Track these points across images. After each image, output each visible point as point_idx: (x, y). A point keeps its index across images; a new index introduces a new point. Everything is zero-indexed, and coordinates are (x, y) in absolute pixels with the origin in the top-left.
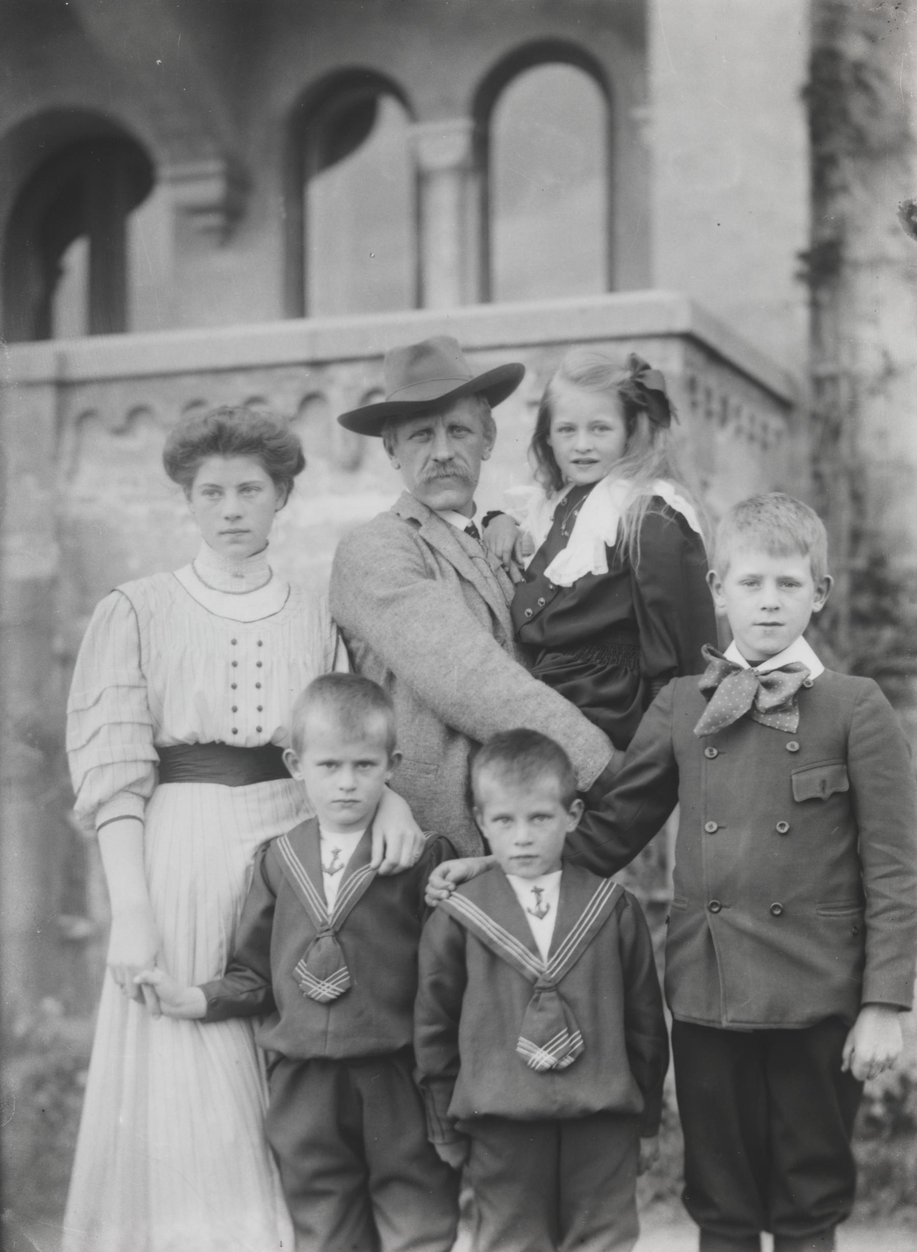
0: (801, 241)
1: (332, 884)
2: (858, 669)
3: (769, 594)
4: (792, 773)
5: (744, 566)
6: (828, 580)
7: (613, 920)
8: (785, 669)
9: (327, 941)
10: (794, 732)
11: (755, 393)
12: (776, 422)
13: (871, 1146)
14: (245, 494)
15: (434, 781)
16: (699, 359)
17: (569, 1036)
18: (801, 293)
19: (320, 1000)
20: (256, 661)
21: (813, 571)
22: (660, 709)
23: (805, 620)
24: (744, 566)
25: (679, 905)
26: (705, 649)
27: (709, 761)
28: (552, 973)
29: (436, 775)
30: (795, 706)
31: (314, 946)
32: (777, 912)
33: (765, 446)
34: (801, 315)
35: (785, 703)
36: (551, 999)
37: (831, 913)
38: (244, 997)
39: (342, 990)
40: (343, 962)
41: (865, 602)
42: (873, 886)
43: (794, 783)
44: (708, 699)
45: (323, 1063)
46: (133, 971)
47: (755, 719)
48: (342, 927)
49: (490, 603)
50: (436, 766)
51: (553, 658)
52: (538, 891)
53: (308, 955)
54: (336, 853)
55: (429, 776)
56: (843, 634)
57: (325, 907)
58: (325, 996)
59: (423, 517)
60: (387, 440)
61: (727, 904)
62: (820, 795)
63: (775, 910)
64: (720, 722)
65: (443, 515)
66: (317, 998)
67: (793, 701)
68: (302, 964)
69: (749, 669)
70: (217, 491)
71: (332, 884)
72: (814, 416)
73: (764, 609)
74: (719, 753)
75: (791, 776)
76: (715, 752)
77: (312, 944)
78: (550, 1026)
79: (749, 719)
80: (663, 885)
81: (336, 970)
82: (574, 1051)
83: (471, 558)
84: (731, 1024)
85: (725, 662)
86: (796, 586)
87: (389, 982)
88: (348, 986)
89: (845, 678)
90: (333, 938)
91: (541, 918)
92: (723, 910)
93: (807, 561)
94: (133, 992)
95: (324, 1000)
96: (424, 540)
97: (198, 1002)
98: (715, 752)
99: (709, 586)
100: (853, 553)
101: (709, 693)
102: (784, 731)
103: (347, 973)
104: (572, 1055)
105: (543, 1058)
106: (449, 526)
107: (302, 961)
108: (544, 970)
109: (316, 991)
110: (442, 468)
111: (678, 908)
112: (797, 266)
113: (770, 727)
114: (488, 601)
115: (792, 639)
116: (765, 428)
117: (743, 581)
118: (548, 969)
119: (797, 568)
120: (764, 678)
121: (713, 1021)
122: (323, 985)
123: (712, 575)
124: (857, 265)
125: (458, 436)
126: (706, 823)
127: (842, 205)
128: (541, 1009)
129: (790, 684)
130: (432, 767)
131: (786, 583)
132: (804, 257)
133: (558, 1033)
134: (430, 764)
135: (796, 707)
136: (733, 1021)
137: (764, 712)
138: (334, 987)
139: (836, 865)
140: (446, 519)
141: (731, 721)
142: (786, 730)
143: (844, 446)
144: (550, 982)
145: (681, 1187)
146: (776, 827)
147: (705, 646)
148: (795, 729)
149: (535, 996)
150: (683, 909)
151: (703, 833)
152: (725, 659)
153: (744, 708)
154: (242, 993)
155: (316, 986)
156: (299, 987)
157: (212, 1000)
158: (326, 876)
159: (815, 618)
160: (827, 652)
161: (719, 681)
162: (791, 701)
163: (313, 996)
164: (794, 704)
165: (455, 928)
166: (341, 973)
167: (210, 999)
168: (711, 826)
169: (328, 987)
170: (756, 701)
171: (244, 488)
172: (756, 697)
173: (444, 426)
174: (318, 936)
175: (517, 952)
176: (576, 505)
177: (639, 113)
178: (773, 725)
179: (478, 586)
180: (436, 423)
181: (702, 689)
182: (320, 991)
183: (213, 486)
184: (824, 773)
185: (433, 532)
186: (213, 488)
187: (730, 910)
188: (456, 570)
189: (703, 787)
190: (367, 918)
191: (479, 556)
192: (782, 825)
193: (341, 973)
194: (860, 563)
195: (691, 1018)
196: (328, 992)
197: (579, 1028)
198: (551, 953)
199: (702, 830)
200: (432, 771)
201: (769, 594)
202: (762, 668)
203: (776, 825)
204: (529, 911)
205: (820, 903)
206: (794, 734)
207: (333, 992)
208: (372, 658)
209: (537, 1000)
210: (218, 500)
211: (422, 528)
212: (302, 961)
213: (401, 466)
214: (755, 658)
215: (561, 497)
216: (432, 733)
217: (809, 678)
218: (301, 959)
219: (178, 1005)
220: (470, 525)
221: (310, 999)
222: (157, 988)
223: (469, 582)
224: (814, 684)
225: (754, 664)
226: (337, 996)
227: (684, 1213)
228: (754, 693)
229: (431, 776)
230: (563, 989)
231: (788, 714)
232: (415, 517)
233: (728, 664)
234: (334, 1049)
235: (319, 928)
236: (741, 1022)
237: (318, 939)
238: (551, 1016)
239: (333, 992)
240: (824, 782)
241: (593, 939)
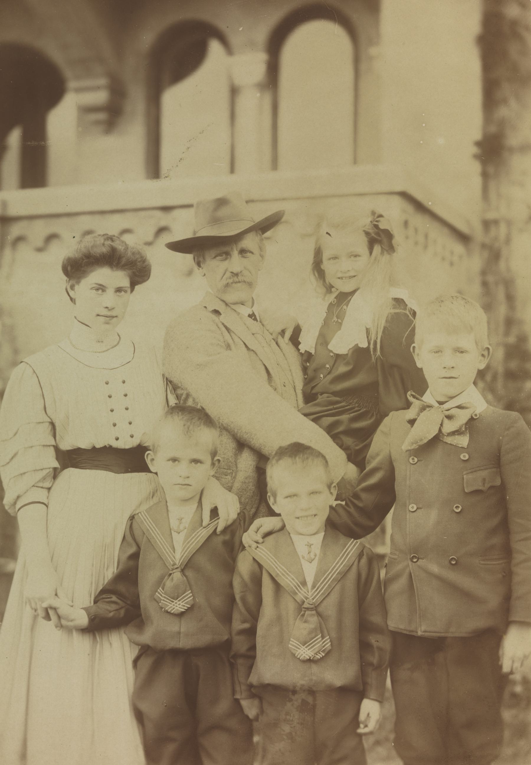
0: (478, 135)
1: (179, 540)
2: (510, 406)
4: (464, 474)
7: (356, 563)
8: (460, 407)
9: (177, 575)
10: (466, 447)
11: (446, 231)
12: (459, 248)
13: (514, 712)
14: (118, 294)
15: (230, 480)
16: (410, 208)
17: (322, 639)
18: (476, 167)
19: (175, 613)
22: (382, 432)
23: (473, 375)
25: (393, 556)
26: (410, 394)
27: (412, 466)
28: (313, 599)
29: (232, 477)
30: (466, 431)
31: (168, 579)
32: (453, 562)
33: (452, 264)
34: (477, 181)
35: (460, 429)
36: (312, 615)
37: (488, 563)
38: (111, 614)
40: (188, 588)
41: (513, 365)
42: (516, 546)
43: (465, 480)
44: (412, 426)
45: (175, 653)
46: (42, 600)
47: (441, 439)
48: (186, 565)
49: (266, 365)
50: (231, 471)
51: (328, 397)
52: (310, 546)
53: (164, 585)
54: (180, 520)
55: (227, 477)
56: (500, 384)
57: (173, 553)
58: (178, 610)
59: (221, 307)
60: (196, 258)
61: (422, 557)
62: (480, 488)
63: (452, 561)
64: (419, 441)
65: (234, 307)
66: (172, 612)
67: (465, 427)
68: (160, 590)
69: (438, 406)
71: (179, 540)
72: (484, 246)
74: (418, 461)
75: (463, 476)
76: (416, 460)
77: (166, 578)
78: (310, 633)
79: (437, 439)
80: (383, 543)
81: (184, 593)
82: (325, 649)
83: (253, 334)
84: (423, 633)
85: (423, 403)
87: (218, 601)
88: (192, 603)
89: (499, 411)
90: (181, 573)
91: (311, 562)
92: (420, 560)
94: (41, 613)
95: (176, 612)
96: (223, 324)
97: (83, 620)
98: (416, 460)
99: (413, 354)
100: (507, 333)
101: (412, 422)
102: (459, 447)
103: (191, 594)
104: (323, 651)
105: (305, 653)
106: (239, 314)
107: (160, 588)
108: (308, 597)
109: (171, 607)
110: (236, 277)
111: (393, 558)
112: (475, 150)
113: (450, 444)
114: (265, 363)
116: (452, 253)
118: (311, 597)
120: (447, 413)
121: (412, 631)
122: (176, 603)
123: (414, 347)
124: (511, 150)
125: (246, 256)
126: (409, 505)
127: (503, 112)
128: (306, 622)
129: (463, 417)
130: (229, 471)
132: (478, 144)
133: (315, 637)
134: (227, 469)
135: (467, 431)
136: (425, 632)
137: (447, 434)
138: (183, 604)
139: (493, 532)
140: (237, 310)
141: (425, 441)
142: (460, 446)
143: (502, 265)
144: (312, 605)
145: (392, 736)
146: (453, 508)
147: (409, 393)
148: (466, 445)
149: (302, 612)
150: (395, 559)
151: (407, 512)
152: (422, 401)
153: (434, 432)
154: (110, 612)
155: (171, 604)
156: (159, 605)
157: (92, 616)
158: (174, 534)
159: (481, 374)
160: (490, 397)
161: (418, 415)
162: (464, 426)
163: (169, 611)
164: (466, 428)
165: (256, 566)
166: (187, 595)
167: (90, 616)
168: (413, 507)
169: (179, 604)
170: (441, 427)
172: (442, 425)
173: (237, 250)
174: (171, 572)
175: (293, 584)
176: (344, 303)
177: (373, 51)
178: (452, 443)
179: (258, 353)
180: (232, 248)
181: (408, 420)
183: (100, 285)
184: (484, 474)
185: (227, 317)
187: (424, 560)
188: (245, 344)
189: (408, 482)
190: (203, 561)
191: (258, 333)
192: (457, 507)
193: (187, 595)
194: (512, 340)
195: (398, 628)
196: (179, 608)
197: (329, 635)
198: (313, 587)
199: (407, 510)
200: (229, 474)
202: (446, 406)
203: (453, 507)
204: (303, 558)
205: (481, 556)
206: (465, 448)
207: (182, 607)
208: (191, 401)
209: (303, 615)
211: (222, 316)
212: (160, 588)
213: (206, 275)
214: (442, 399)
215: (331, 298)
216: (228, 449)
217: (476, 412)
218: (160, 587)
219: (72, 621)
220: (251, 313)
221: (167, 612)
222: (58, 610)
223: (253, 350)
224: (480, 416)
225: (441, 403)
226: (185, 609)
227: (394, 753)
228: (440, 423)
229: (229, 477)
230: (320, 609)
231: (462, 435)
232: (217, 309)
233: (424, 405)
234: (184, 643)
235: (170, 567)
236: (430, 632)
237: (171, 574)
238: (312, 626)
239: (182, 607)
240: (484, 480)
241: (341, 578)
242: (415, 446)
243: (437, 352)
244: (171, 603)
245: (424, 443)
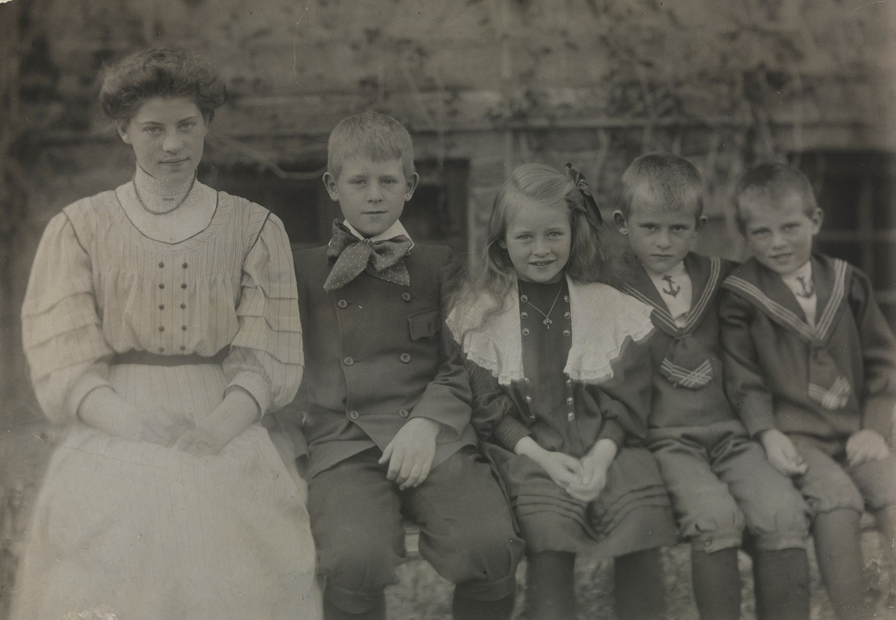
3: (374, 190)
5: (353, 169)
6: (415, 176)
8: (394, 240)
14: (183, 128)
20: (181, 282)
21: (405, 170)
24: (353, 169)
39: (710, 378)
70: (159, 128)
73: (371, 201)
86: (393, 182)
93: (400, 162)
101: (333, 260)
102: (387, 281)
109: (687, 380)
115: (391, 224)
117: (352, 181)
119: (393, 169)
131: (386, 180)
138: (703, 375)
155: (686, 376)
169: (698, 376)
171: (183, 124)
182: (690, 380)
183: (154, 123)
186: (153, 126)
201: (374, 190)
210: (158, 135)
242: (338, 285)
243: (359, 182)
244: (686, 374)
245: (349, 281)
